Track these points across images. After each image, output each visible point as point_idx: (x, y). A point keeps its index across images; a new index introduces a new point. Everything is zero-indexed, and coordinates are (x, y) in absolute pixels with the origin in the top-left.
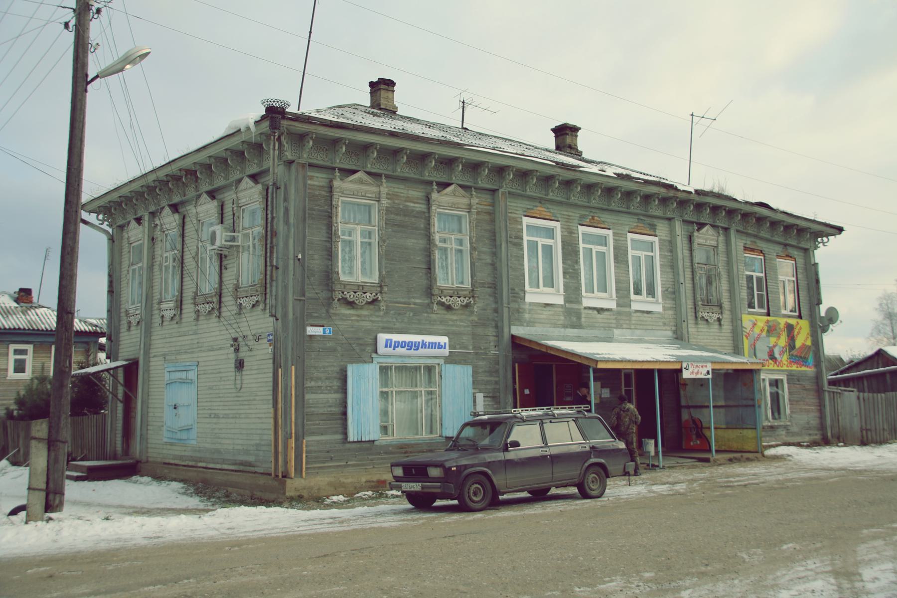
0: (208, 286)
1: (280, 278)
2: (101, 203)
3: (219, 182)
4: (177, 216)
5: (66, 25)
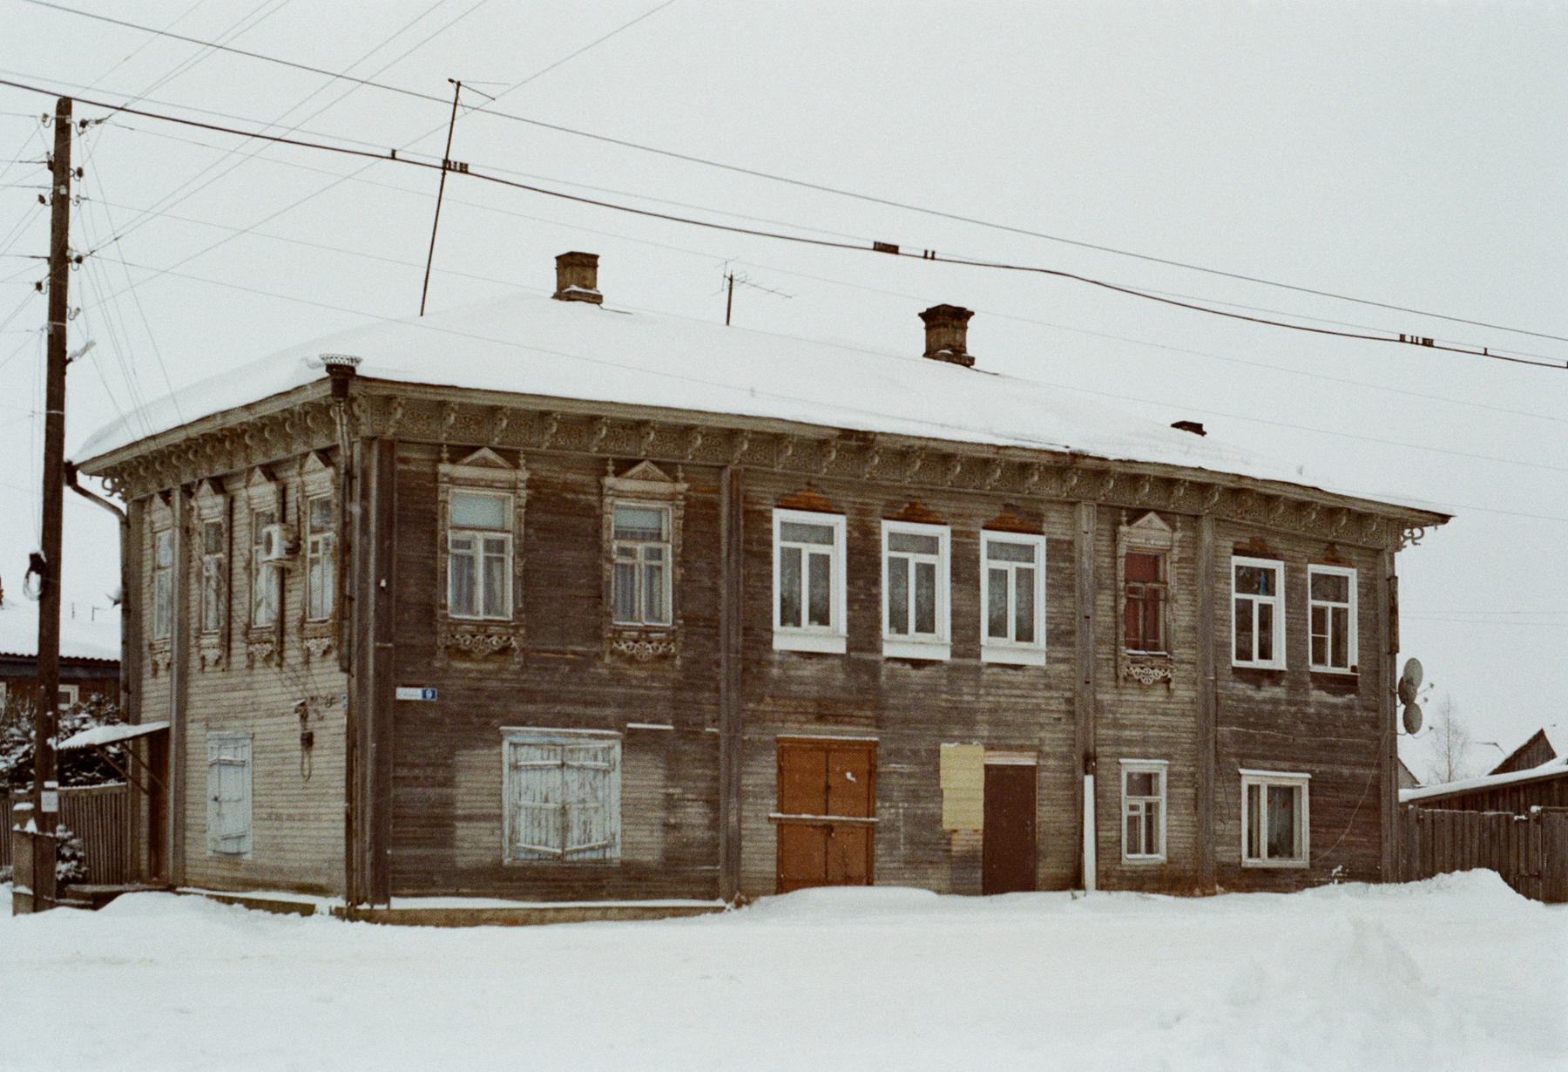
0: (264, 617)
1: (355, 616)
2: (108, 462)
3: (278, 454)
4: (220, 499)
5: (39, 286)
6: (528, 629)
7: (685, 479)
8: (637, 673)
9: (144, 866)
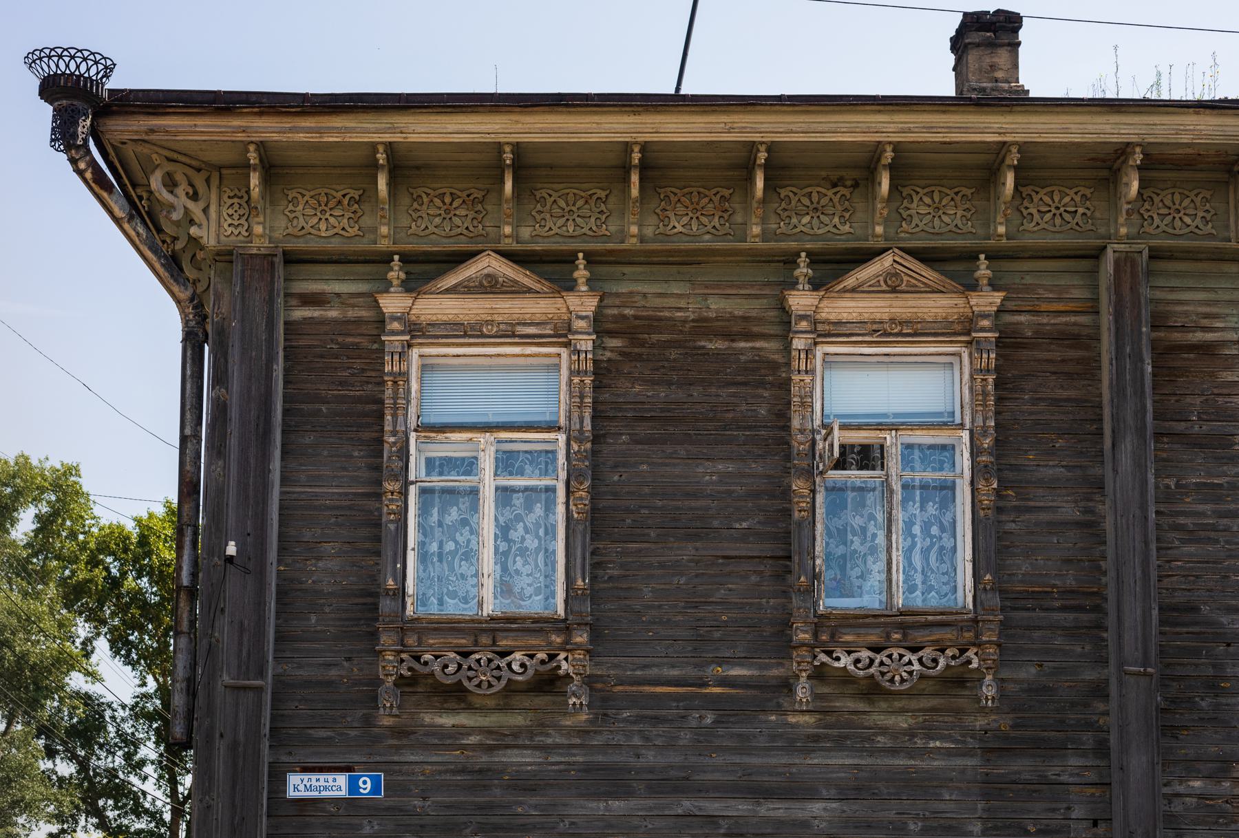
6: (596, 635)
7: (994, 286)
8: (890, 721)
9: (375, 407)
